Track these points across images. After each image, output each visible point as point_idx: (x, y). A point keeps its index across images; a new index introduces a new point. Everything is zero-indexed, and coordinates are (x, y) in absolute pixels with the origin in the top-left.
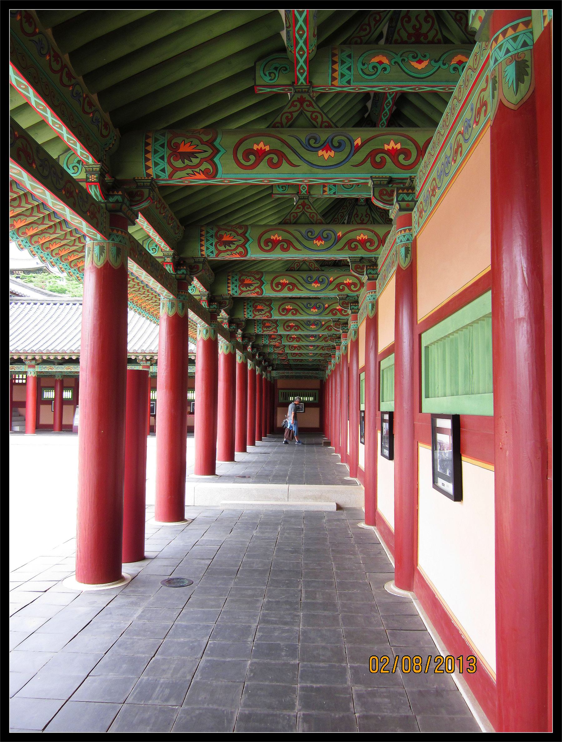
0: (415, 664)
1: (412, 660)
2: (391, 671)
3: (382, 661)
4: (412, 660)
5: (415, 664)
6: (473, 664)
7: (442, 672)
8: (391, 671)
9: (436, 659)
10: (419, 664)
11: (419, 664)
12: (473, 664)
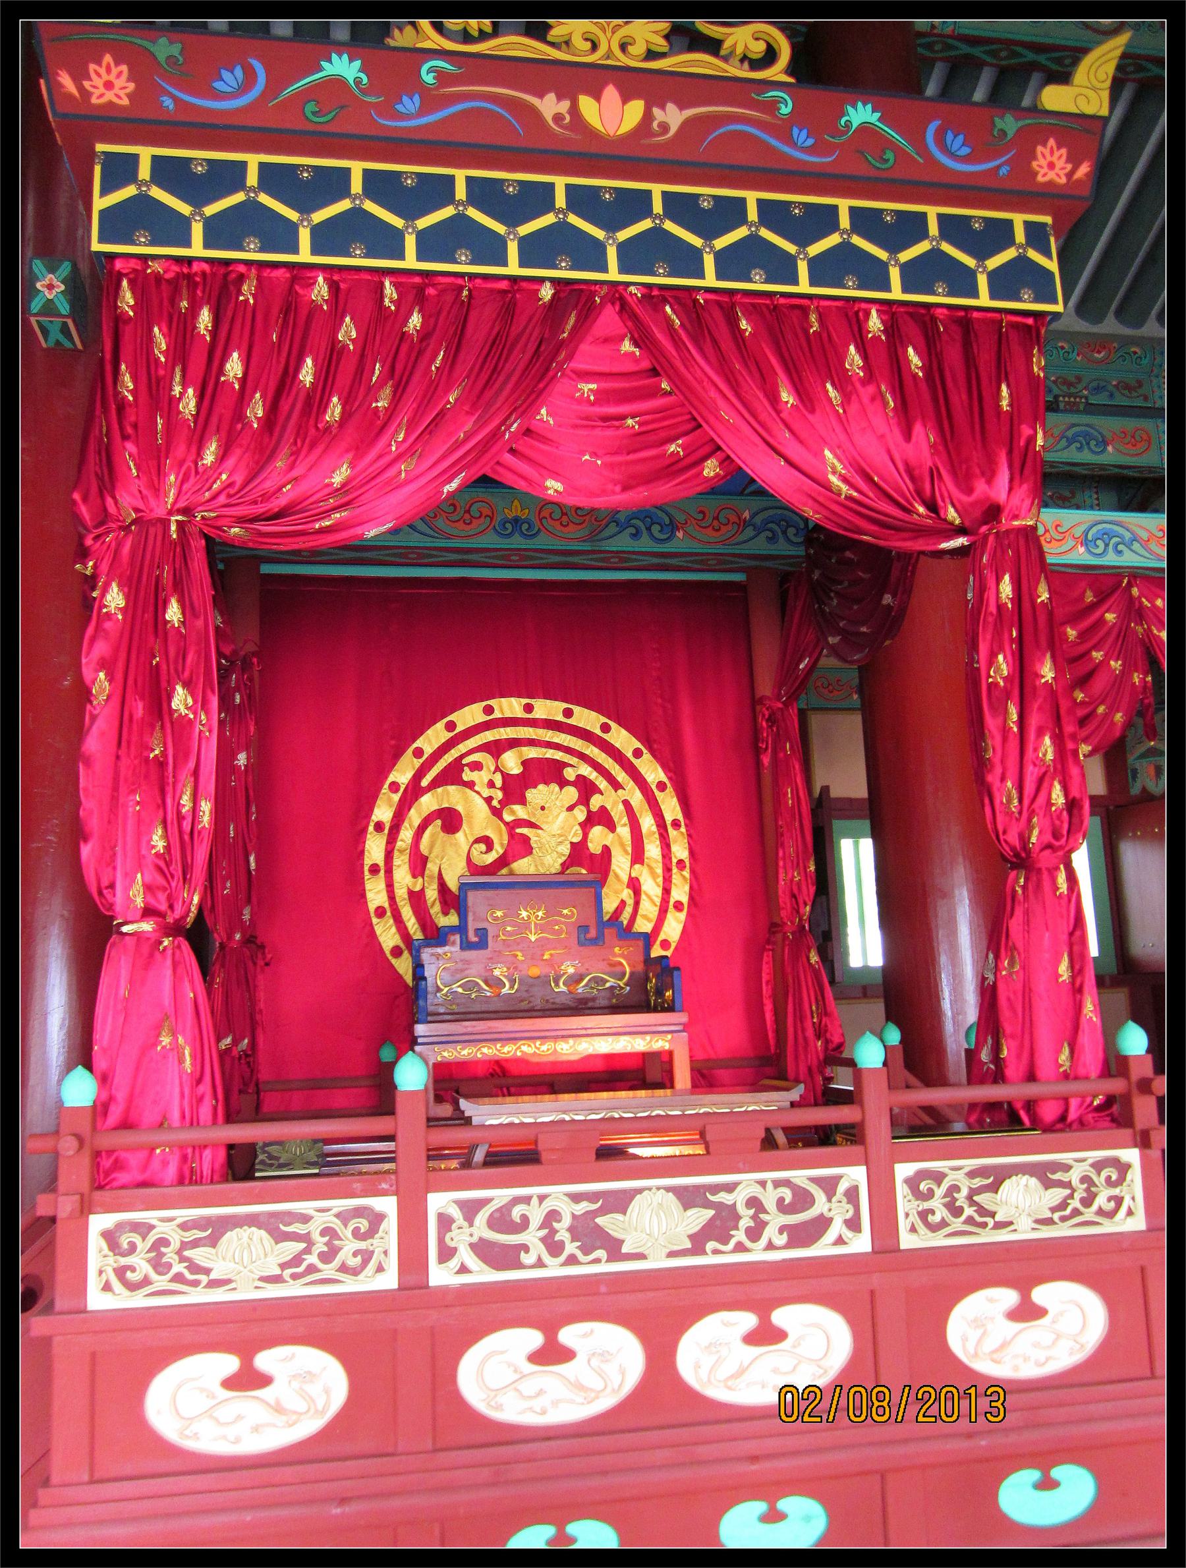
0: (876, 1404)
1: (869, 1397)
2: (825, 1417)
3: (805, 1396)
4: (869, 1397)
5: (876, 1404)
6: (998, 1404)
7: (933, 1419)
8: (825, 1417)
9: (921, 1392)
10: (885, 1404)
11: (885, 1404)
12: (998, 1404)
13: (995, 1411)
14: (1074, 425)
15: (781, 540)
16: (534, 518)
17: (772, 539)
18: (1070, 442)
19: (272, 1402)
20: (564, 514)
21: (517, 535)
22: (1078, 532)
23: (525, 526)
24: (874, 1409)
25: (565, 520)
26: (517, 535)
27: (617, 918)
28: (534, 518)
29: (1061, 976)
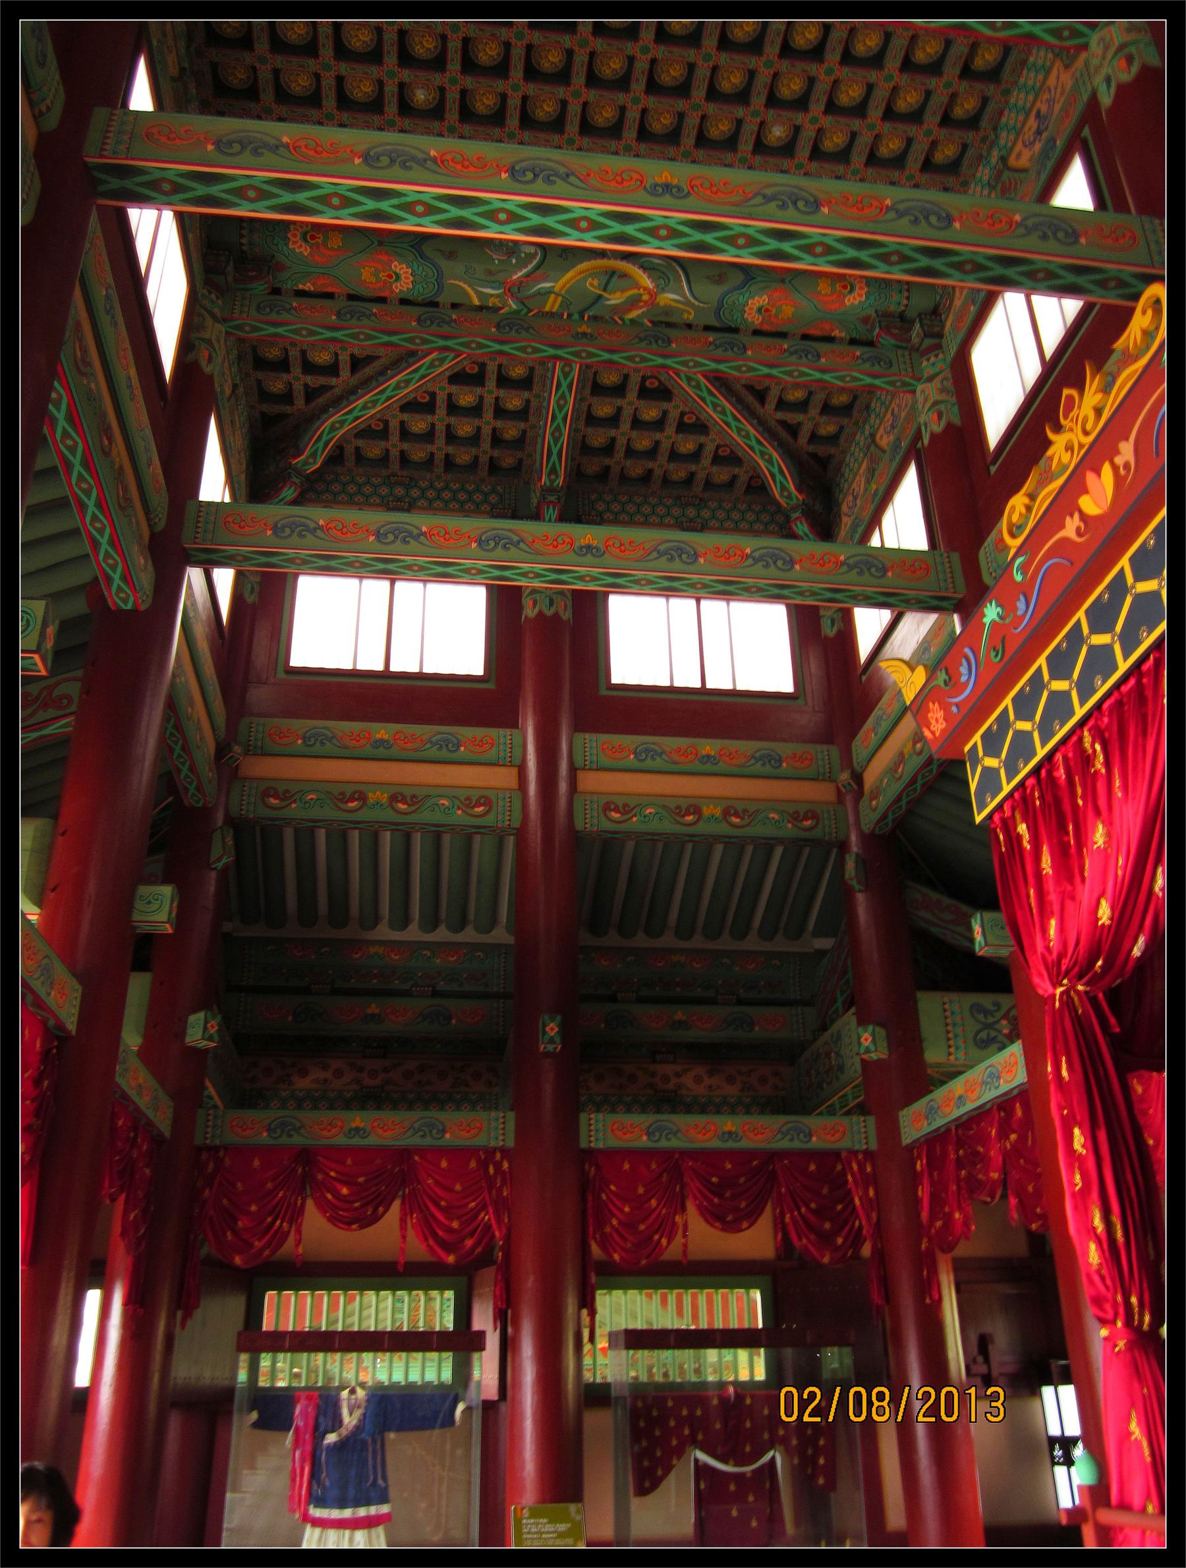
5: (876, 1404)
10: (885, 1404)
12: (998, 1404)
13: (995, 1412)
14: (787, 1123)
15: (867, 574)
16: (601, 546)
17: (861, 573)
18: (785, 1135)
20: (447, 533)
21: (589, 555)
22: (644, 1127)
23: (594, 551)
24: (874, 1410)
25: (447, 536)
26: (589, 555)
27: (1079, 135)
28: (601, 546)
29: (1133, 1433)
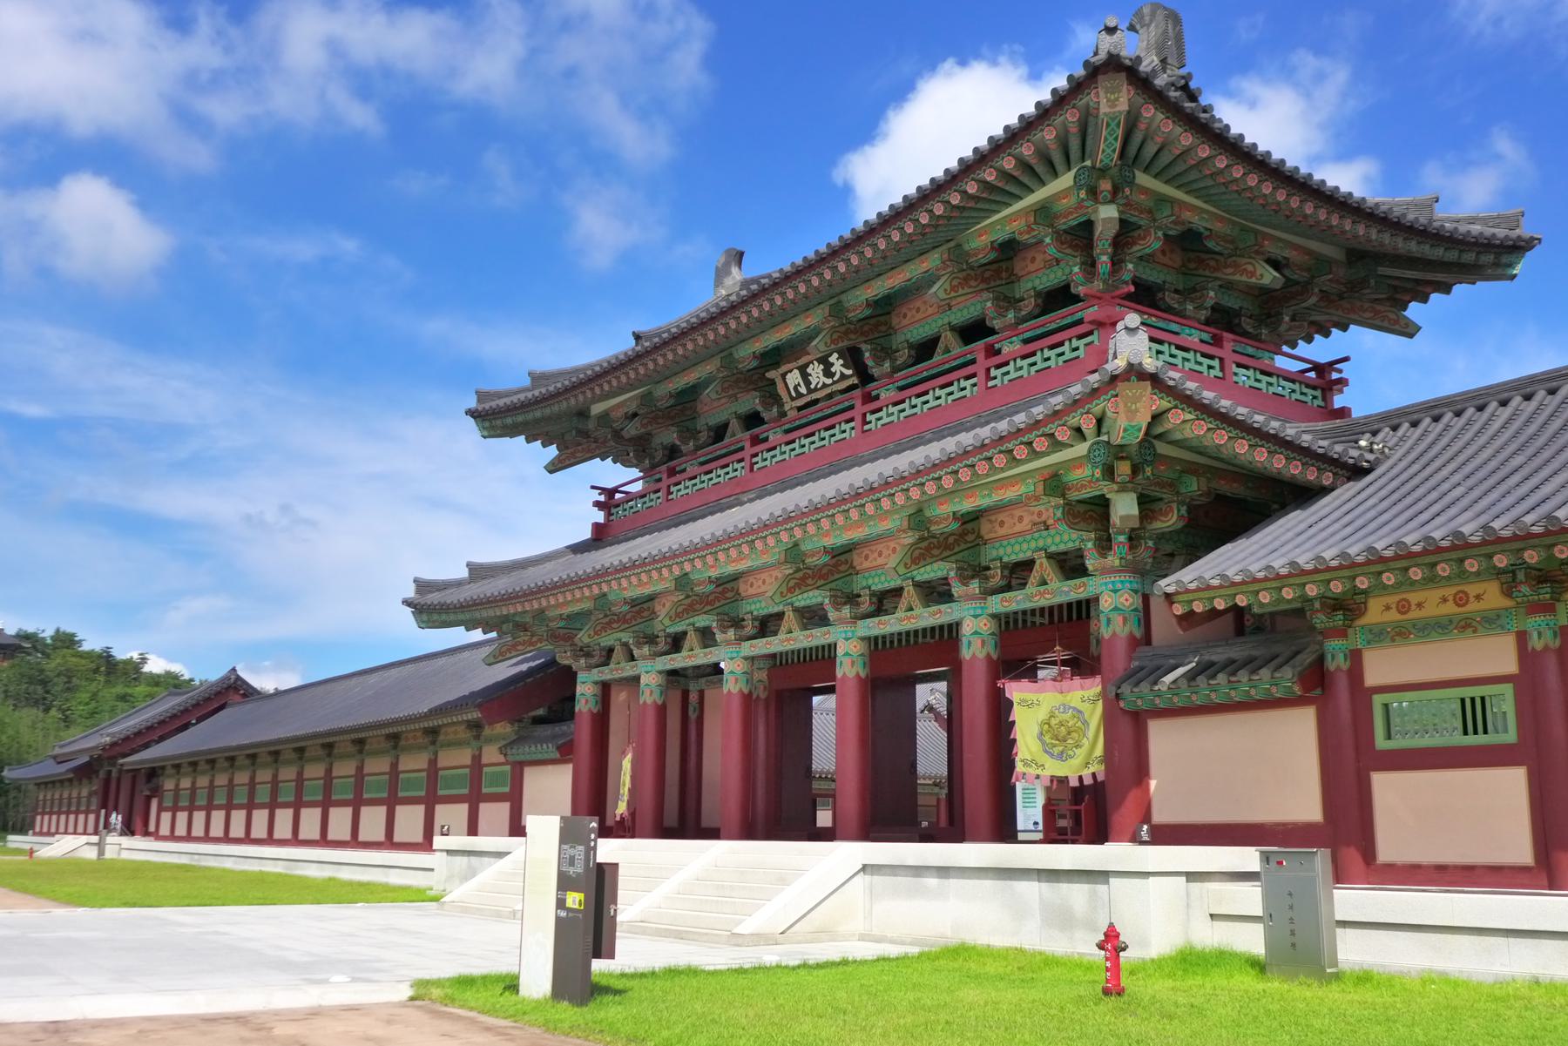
19: (464, 573)
